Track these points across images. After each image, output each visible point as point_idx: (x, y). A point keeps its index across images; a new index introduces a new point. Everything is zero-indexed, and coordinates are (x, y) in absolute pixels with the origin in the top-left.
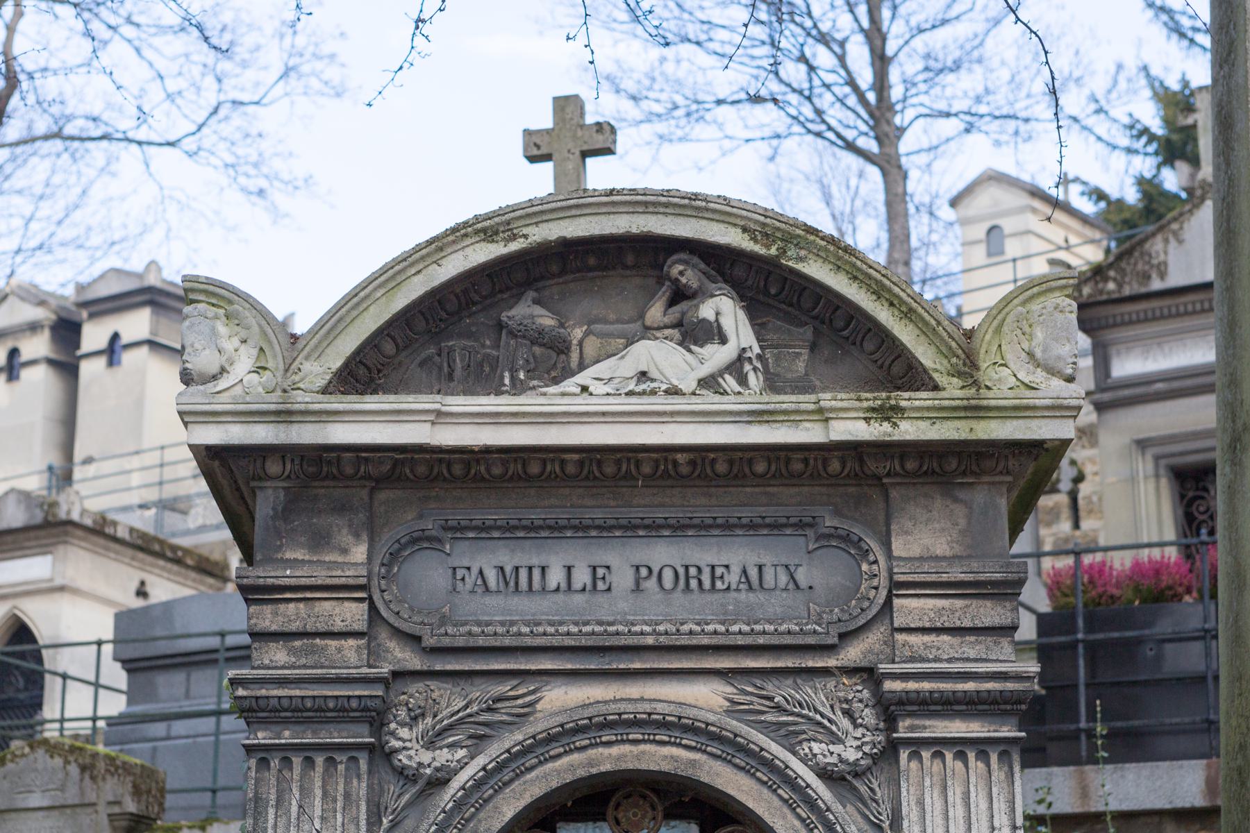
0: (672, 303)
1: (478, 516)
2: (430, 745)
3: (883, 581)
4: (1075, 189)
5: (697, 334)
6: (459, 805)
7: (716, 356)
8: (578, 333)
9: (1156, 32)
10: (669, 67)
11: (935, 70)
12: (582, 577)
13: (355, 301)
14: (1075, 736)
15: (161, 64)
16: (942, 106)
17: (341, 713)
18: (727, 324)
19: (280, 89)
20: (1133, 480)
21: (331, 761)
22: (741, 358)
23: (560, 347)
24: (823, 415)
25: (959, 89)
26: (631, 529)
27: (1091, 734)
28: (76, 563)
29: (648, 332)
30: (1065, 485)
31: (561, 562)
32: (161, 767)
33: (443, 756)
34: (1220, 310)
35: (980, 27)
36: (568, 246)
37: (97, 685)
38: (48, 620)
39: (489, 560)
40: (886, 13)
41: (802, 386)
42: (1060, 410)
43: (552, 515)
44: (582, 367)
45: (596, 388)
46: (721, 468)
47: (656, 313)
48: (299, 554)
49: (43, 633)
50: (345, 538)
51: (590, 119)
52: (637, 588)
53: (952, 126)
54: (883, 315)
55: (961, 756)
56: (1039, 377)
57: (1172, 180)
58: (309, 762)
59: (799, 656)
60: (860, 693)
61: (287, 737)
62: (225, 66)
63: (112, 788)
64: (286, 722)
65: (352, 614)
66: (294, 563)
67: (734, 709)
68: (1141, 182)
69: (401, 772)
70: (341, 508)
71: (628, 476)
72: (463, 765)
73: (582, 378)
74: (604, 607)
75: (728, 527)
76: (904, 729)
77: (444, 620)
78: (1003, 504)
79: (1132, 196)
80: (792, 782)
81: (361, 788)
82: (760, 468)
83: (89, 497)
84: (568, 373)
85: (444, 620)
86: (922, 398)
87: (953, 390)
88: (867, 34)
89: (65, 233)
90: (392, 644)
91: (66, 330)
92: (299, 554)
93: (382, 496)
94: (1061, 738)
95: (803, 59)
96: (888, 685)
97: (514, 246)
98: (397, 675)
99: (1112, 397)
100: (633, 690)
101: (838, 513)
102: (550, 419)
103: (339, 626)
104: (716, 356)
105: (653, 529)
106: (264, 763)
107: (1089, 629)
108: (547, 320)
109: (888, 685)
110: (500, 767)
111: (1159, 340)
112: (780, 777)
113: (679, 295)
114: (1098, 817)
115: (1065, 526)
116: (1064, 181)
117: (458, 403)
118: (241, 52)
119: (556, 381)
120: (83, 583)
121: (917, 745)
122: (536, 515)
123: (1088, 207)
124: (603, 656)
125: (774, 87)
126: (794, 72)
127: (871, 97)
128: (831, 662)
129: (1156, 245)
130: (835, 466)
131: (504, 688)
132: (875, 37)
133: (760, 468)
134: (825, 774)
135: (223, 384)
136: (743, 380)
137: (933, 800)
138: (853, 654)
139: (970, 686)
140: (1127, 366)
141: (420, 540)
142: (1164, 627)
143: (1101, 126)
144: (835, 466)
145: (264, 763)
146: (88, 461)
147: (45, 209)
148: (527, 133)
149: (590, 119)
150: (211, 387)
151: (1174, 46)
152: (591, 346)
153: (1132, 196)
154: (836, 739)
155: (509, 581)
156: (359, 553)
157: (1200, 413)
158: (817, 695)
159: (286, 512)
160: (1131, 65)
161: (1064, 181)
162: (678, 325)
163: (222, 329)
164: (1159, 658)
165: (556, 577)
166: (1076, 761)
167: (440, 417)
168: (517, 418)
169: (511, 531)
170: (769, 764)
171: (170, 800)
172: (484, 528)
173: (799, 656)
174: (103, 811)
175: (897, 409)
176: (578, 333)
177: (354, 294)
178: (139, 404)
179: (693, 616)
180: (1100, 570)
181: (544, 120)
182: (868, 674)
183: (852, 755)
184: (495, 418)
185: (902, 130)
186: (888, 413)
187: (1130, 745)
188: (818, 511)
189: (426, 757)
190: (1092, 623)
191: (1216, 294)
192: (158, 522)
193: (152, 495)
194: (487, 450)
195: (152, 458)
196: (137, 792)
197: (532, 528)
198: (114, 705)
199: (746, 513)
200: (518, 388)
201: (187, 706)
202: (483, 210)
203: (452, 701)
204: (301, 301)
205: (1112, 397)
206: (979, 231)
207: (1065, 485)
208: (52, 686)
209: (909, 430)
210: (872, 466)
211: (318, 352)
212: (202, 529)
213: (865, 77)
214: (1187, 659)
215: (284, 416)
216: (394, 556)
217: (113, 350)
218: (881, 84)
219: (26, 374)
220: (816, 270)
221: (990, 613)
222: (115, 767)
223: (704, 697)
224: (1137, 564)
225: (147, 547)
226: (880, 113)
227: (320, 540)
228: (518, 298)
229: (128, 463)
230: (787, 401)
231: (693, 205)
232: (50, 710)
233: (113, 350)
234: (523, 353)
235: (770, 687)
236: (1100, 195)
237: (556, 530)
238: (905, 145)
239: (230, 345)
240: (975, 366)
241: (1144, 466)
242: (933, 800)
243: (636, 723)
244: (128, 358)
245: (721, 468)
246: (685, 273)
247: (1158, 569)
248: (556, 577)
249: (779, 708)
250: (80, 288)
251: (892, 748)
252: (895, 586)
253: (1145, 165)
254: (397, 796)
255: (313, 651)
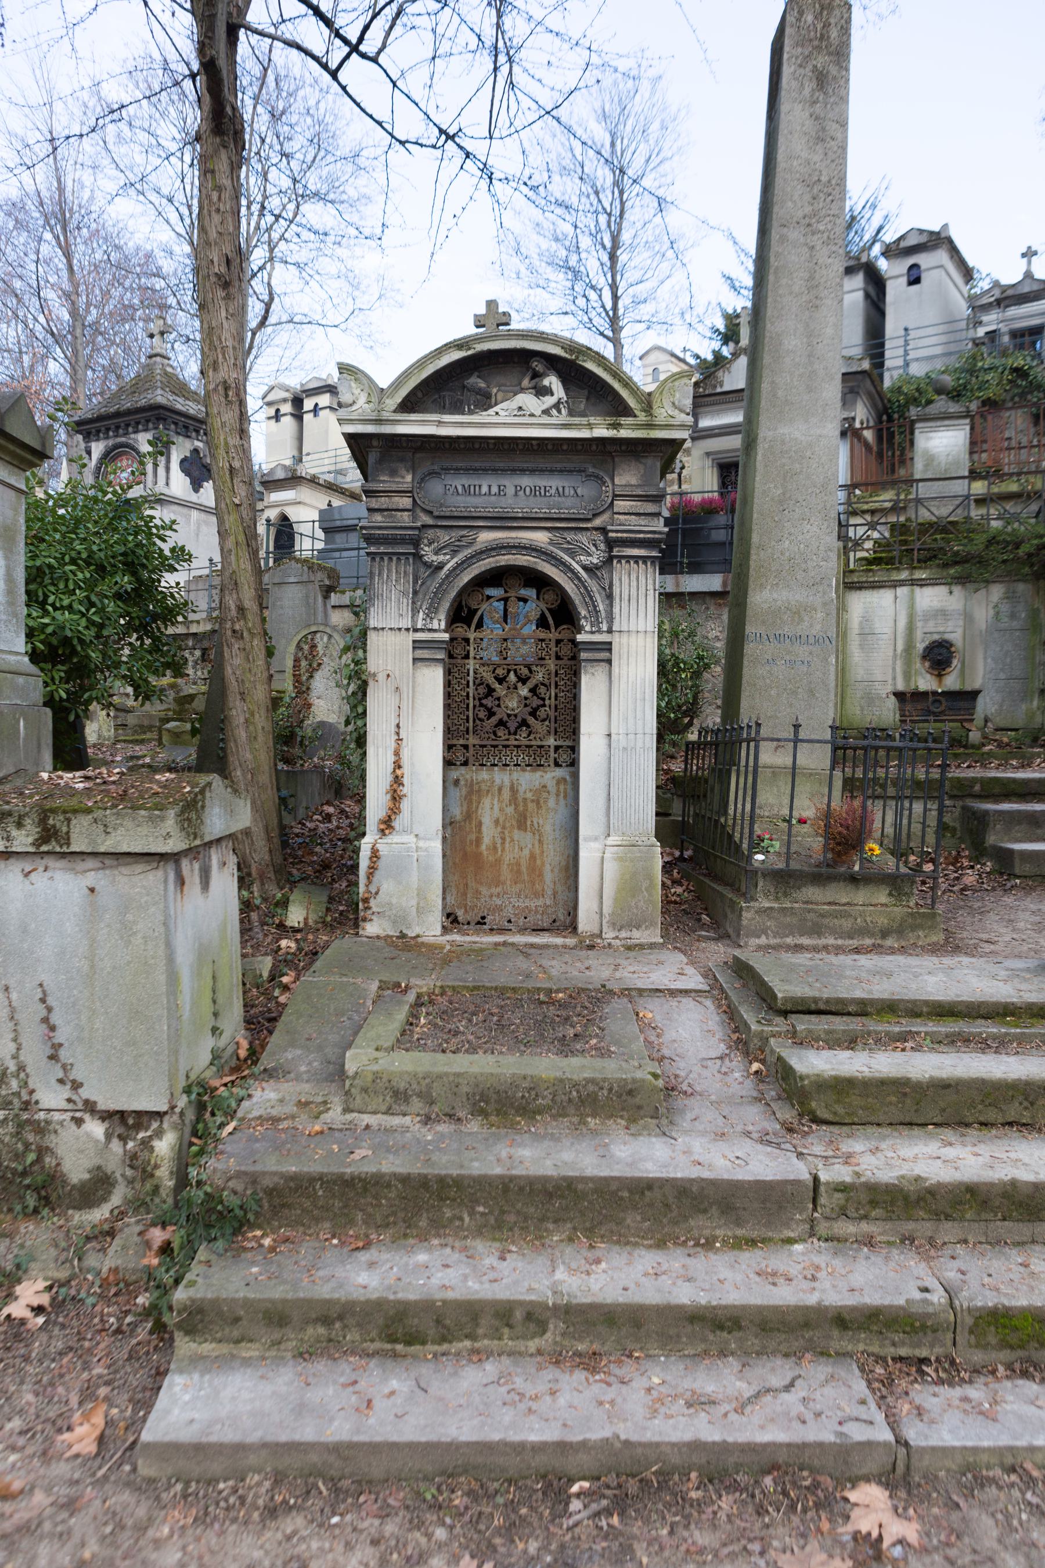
0: (532, 378)
1: (455, 465)
2: (436, 553)
3: (610, 494)
4: (688, 354)
5: (543, 392)
6: (447, 576)
7: (549, 401)
8: (495, 390)
9: (726, 288)
10: (532, 298)
11: (637, 302)
12: (495, 490)
13: (406, 375)
14: (675, 564)
15: (331, 293)
16: (638, 318)
17: (402, 541)
18: (554, 388)
19: (378, 304)
20: (703, 468)
21: (399, 559)
22: (559, 402)
23: (488, 396)
24: (590, 426)
25: (645, 311)
26: (514, 471)
27: (682, 563)
28: (304, 493)
29: (522, 390)
30: (677, 470)
31: (487, 484)
32: (338, 568)
33: (441, 558)
34: (744, 403)
35: (656, 284)
36: (491, 352)
37: (313, 538)
38: (294, 514)
39: (459, 482)
40: (618, 277)
41: (583, 415)
42: (682, 426)
43: (483, 465)
44: (496, 404)
45: (501, 413)
46: (550, 447)
47: (526, 382)
48: (386, 478)
49: (293, 518)
50: (403, 472)
51: (501, 310)
52: (516, 494)
53: (643, 326)
54: (616, 385)
55: (637, 562)
56: (676, 413)
57: (726, 351)
58: (391, 559)
59: (576, 523)
60: (599, 537)
61: (382, 549)
62: (356, 293)
63: (320, 575)
64: (382, 544)
65: (406, 502)
66: (384, 482)
67: (551, 542)
68: (714, 351)
69: (425, 564)
70: (402, 460)
71: (513, 450)
72: (448, 561)
73: (496, 409)
74: (503, 502)
75: (552, 471)
76: (615, 552)
77: (441, 505)
78: (658, 465)
79: (710, 357)
80: (572, 571)
81: (410, 569)
82: (565, 447)
83: (309, 467)
84: (491, 407)
85: (441, 505)
86: (630, 420)
87: (642, 417)
88: (611, 286)
89: (296, 363)
90: (421, 514)
91: (297, 402)
92: (386, 478)
93: (418, 455)
94: (669, 564)
95: (584, 296)
96: (611, 535)
97: (470, 353)
98: (424, 526)
99: (699, 435)
100: (513, 534)
101: (594, 467)
102: (483, 425)
103: (401, 507)
104: (549, 401)
105: (523, 471)
106: (373, 559)
107: (684, 523)
108: (482, 385)
109: (611, 535)
110: (463, 562)
111: (719, 412)
112: (568, 569)
113: (536, 375)
114: (682, 594)
115: (675, 488)
116: (685, 350)
117: (447, 418)
118: (362, 287)
119: (486, 410)
120: (307, 501)
121: (620, 558)
122: (477, 465)
123: (692, 361)
124: (502, 521)
125: (573, 308)
126: (581, 302)
127: (611, 313)
128: (589, 525)
129: (720, 374)
130: (594, 447)
131: (464, 532)
132: (614, 287)
133: (565, 447)
134: (585, 568)
135: (354, 408)
136: (559, 412)
137: (625, 579)
138: (597, 522)
139: (642, 536)
140: (705, 423)
141: (433, 474)
142: (711, 524)
143: (700, 328)
144: (594, 447)
145: (373, 559)
146: (308, 454)
147: (287, 353)
148: (476, 316)
149: (501, 310)
150: (350, 409)
151: (732, 294)
152: (500, 396)
153: (710, 357)
154: (590, 555)
155: (467, 491)
156: (409, 478)
157: (735, 442)
158: (583, 538)
159: (380, 461)
160: (714, 303)
161: (685, 350)
162: (534, 388)
163: (353, 385)
164: (709, 535)
165: (485, 489)
166: (676, 573)
167: (440, 423)
168: (470, 424)
169: (469, 471)
170: (564, 564)
171: (342, 581)
172: (457, 469)
173: (576, 523)
174: (317, 584)
175: (620, 425)
176: (495, 390)
177: (406, 371)
178: (327, 432)
179: (538, 506)
180: (689, 502)
181: (482, 310)
182: (603, 530)
183: (595, 561)
184: (461, 424)
185: (622, 328)
186: (616, 426)
187: (696, 568)
188: (587, 465)
189: (435, 558)
190: (684, 522)
191: (745, 393)
192: (335, 478)
193: (332, 468)
194: (459, 438)
195: (333, 453)
196: (329, 577)
197: (476, 470)
198: (320, 545)
199: (559, 466)
200: (471, 412)
201: (347, 546)
202: (457, 337)
203: (445, 537)
204: (384, 381)
205: (699, 435)
206: (650, 370)
207: (677, 470)
208: (297, 537)
209: (624, 433)
210: (609, 448)
211: (392, 396)
212: (352, 482)
213: (609, 305)
214: (719, 536)
215: (379, 421)
216: (422, 479)
217: (316, 410)
218: (615, 308)
219: (282, 419)
220: (590, 366)
221: (651, 508)
222: (321, 568)
223: (540, 538)
224: (703, 499)
225: (331, 487)
226: (614, 321)
227: (393, 473)
228: (471, 375)
229: (323, 455)
230: (577, 420)
231: (542, 337)
232: (297, 547)
233: (316, 410)
234: (473, 398)
235: (566, 534)
236: (697, 357)
237: (485, 471)
238: (624, 334)
239: (357, 391)
240: (651, 408)
241: (708, 463)
242: (625, 579)
243: (514, 547)
244: (322, 413)
245: (550, 447)
246: (538, 366)
247: (711, 501)
248: (485, 489)
249: (569, 543)
250: (302, 385)
251: (609, 560)
252: (615, 496)
253: (716, 345)
254: (424, 573)
255: (391, 516)
